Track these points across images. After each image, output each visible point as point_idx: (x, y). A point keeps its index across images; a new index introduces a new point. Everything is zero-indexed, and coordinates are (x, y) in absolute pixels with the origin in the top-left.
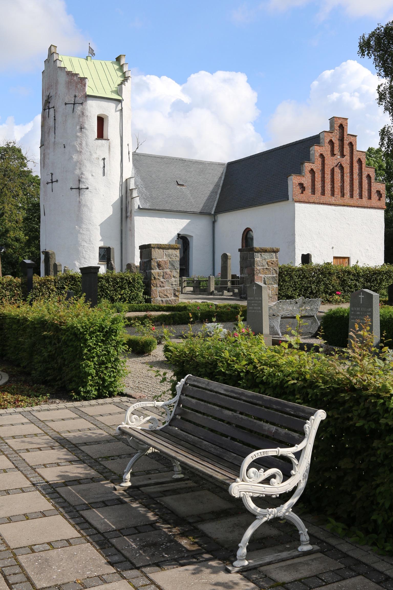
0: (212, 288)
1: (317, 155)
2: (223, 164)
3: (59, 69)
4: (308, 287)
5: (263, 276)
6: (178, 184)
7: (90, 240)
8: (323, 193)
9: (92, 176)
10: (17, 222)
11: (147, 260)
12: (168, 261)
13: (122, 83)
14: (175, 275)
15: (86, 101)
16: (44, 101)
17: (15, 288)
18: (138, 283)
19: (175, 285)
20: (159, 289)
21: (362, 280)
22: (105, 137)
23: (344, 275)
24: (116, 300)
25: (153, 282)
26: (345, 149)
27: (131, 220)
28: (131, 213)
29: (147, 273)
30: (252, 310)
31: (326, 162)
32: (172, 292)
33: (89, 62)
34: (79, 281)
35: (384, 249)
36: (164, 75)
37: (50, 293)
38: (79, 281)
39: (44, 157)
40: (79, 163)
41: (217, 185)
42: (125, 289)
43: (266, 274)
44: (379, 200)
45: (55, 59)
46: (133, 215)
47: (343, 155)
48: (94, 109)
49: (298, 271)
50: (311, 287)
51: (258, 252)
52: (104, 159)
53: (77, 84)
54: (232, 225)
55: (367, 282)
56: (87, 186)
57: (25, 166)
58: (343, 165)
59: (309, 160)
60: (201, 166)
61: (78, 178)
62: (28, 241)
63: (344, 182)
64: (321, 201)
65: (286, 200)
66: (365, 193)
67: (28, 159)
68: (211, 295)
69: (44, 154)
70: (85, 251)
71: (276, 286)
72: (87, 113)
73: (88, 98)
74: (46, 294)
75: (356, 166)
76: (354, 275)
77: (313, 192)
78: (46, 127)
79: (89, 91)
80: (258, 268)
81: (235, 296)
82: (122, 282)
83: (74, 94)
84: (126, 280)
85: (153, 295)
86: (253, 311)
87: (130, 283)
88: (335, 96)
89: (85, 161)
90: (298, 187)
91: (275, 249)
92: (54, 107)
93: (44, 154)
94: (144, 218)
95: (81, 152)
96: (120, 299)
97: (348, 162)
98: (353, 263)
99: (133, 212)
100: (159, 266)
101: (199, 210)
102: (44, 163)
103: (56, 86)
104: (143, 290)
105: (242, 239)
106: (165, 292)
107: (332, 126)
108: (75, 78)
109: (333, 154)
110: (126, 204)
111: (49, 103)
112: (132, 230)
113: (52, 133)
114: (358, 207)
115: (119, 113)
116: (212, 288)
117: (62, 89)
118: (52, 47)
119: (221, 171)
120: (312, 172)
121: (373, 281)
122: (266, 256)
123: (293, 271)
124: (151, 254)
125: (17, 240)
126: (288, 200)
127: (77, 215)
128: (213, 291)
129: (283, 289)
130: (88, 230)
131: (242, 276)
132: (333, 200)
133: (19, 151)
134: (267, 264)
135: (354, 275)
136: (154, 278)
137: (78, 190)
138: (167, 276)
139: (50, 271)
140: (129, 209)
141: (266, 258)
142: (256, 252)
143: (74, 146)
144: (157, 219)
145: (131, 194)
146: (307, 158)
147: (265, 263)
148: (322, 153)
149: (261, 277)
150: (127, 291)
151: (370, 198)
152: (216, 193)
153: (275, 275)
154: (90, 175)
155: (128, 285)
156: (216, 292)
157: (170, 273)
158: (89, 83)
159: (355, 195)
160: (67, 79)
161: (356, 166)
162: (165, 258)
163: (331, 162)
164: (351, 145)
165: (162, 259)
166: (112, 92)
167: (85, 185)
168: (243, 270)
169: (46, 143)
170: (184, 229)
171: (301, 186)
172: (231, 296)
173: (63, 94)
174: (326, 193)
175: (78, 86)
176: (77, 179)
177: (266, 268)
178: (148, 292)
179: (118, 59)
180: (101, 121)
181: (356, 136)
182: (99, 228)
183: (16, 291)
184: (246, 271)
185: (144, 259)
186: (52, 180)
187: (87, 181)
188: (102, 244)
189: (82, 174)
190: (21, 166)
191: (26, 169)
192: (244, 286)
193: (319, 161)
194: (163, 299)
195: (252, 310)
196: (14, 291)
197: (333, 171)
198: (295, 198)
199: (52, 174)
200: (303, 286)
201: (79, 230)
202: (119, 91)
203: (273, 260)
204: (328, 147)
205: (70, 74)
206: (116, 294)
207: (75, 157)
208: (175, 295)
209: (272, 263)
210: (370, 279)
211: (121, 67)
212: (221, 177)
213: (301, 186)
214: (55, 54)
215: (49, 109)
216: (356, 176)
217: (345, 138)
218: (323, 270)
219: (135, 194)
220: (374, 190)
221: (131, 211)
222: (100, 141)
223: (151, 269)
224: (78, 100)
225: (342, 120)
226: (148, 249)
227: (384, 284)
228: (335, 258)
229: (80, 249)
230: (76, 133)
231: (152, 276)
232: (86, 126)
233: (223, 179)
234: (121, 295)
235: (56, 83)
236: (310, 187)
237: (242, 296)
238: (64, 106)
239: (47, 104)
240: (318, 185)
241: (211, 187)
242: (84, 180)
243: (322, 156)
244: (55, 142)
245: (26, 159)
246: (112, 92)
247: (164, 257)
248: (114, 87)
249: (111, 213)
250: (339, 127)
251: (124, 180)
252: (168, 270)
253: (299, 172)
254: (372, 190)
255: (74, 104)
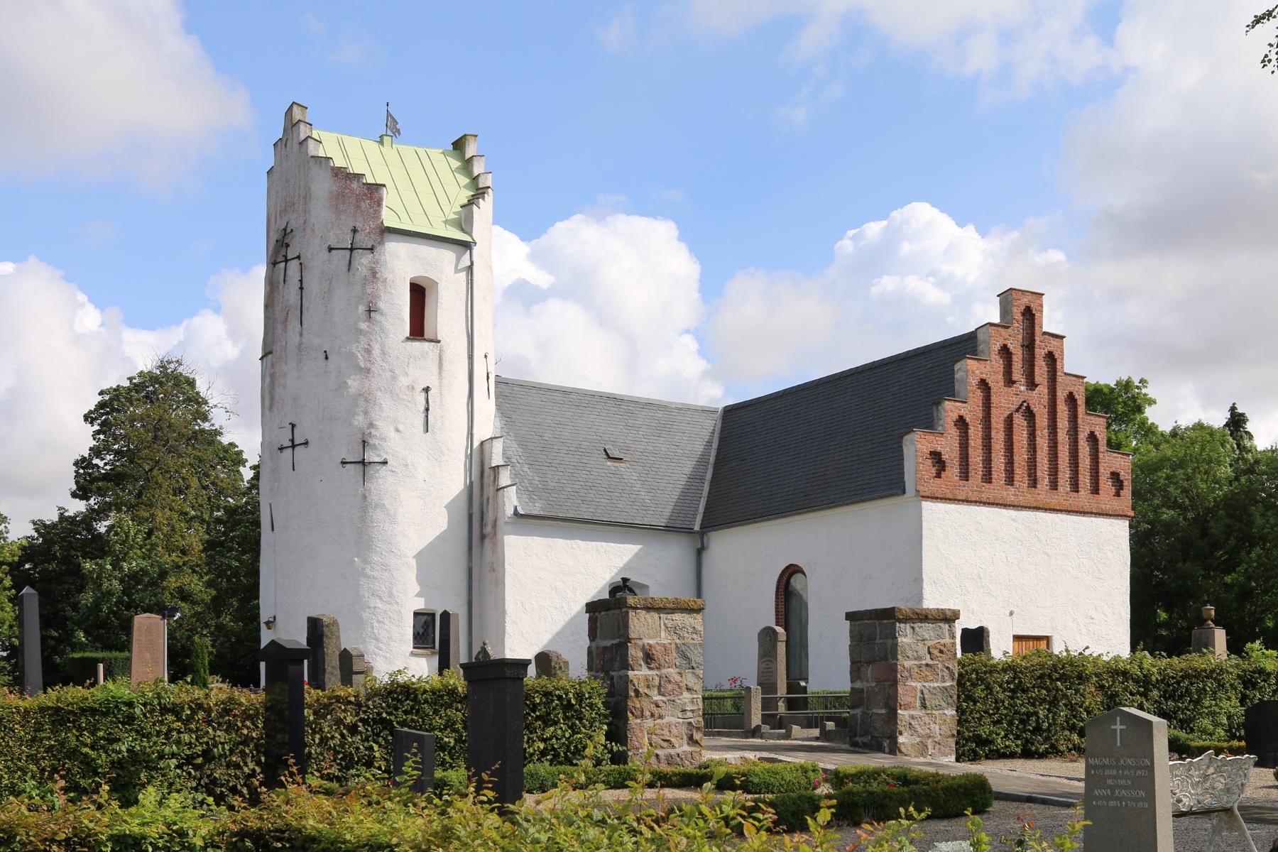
0: (756, 719)
1: (974, 381)
2: (714, 411)
3: (313, 161)
4: (1029, 715)
5: (919, 685)
6: (609, 457)
7: (391, 594)
8: (988, 477)
9: (397, 434)
10: (184, 552)
11: (615, 642)
12: (673, 646)
13: (471, 202)
14: (690, 685)
15: (381, 243)
16: (273, 242)
17: (243, 722)
18: (591, 706)
19: (693, 711)
20: (649, 723)
21: (1155, 693)
22: (428, 333)
23: (1114, 682)
24: (532, 755)
25: (633, 703)
26: (1037, 369)
27: (495, 544)
28: (494, 526)
29: (612, 678)
30: (1108, 798)
31: (994, 399)
32: (684, 730)
33: (386, 149)
34: (426, 701)
35: (1129, 616)
36: (920, 199)
37: (342, 735)
38: (426, 701)
39: (273, 382)
40: (366, 398)
41: (702, 461)
42: (556, 723)
43: (925, 679)
44: (1118, 494)
45: (302, 137)
46: (499, 532)
47: (1032, 385)
48: (402, 263)
49: (1004, 670)
50: (1036, 713)
51: (906, 620)
52: (427, 390)
53: (359, 198)
54: (749, 558)
55: (1166, 699)
56: (385, 456)
57: (205, 419)
58: (1032, 407)
59: (954, 396)
60: (660, 414)
61: (360, 436)
62: (214, 599)
63: (1035, 451)
64: (984, 497)
65: (898, 495)
66: (1085, 479)
67: (211, 403)
68: (753, 737)
69: (272, 375)
70: (379, 622)
71: (951, 712)
72: (384, 273)
73: (387, 236)
74: (333, 738)
75: (1062, 409)
76: (1136, 681)
77: (965, 475)
78: (278, 308)
79: (389, 220)
80: (907, 664)
81: (827, 741)
82: (547, 704)
83: (351, 225)
84: (560, 698)
85: (633, 741)
86: (1112, 803)
87: (569, 706)
88: (888, 283)
89: (379, 393)
90: (929, 462)
91: (949, 614)
92: (299, 257)
93: (272, 375)
94: (529, 539)
95: (368, 371)
96: (543, 753)
97: (1045, 400)
98: (1057, 649)
99: (500, 523)
100: (649, 658)
101: (662, 522)
102: (272, 398)
103: (305, 203)
104: (605, 727)
105: (777, 591)
106: (666, 732)
107: (1005, 311)
108: (355, 185)
109: (1010, 382)
110: (482, 504)
111: (287, 245)
112: (497, 569)
113: (294, 323)
114: (1069, 512)
115: (463, 275)
116: (756, 719)
117: (320, 211)
118: (295, 107)
119: (707, 429)
120: (961, 423)
121: (1181, 697)
122: (926, 630)
123: (991, 672)
124: (626, 626)
125: (184, 595)
126: (904, 492)
127: (359, 529)
128: (758, 727)
129: (966, 721)
130: (386, 567)
131: (858, 685)
132: (1009, 494)
133: (192, 383)
134: (929, 653)
135: (1136, 681)
136: (637, 691)
137: (360, 467)
138: (670, 687)
139: (324, 670)
140: (489, 517)
141: (927, 636)
142: (900, 621)
143: (351, 355)
144: (560, 543)
145: (496, 478)
146: (948, 389)
147: (923, 651)
148: (984, 376)
149: (914, 689)
150: (562, 730)
151: (1095, 490)
152: (702, 479)
153: (948, 684)
154: (392, 429)
155: (564, 713)
156: (766, 729)
157: (678, 678)
158: (389, 198)
159: (1061, 482)
160: (335, 188)
161: (1062, 409)
162: (665, 638)
163: (1005, 401)
164: (1051, 359)
165: (658, 640)
166: (446, 222)
167: (379, 456)
168: (859, 669)
169: (277, 348)
170: (627, 567)
171: (936, 457)
172: (817, 739)
173: (323, 224)
174: (995, 475)
175: (363, 205)
176: (359, 438)
177: (927, 665)
178: (618, 733)
179: (459, 145)
180: (419, 293)
181: (1062, 337)
182: (413, 562)
183: (245, 732)
184: (869, 672)
185: (604, 638)
186: (292, 440)
187: (384, 444)
188: (420, 605)
189: (371, 425)
190: (195, 419)
191: (206, 426)
192: (863, 713)
193: (976, 397)
194: (659, 752)
195: (1108, 798)
196: (239, 729)
197: (1009, 421)
198: (921, 488)
199: (293, 426)
200: (1016, 712)
201: (363, 569)
202: (464, 222)
203: (942, 641)
204: (997, 363)
205: (342, 175)
206: (529, 738)
207: (353, 383)
208: (692, 741)
209: (941, 652)
210: (1175, 690)
211: (467, 164)
212: (710, 443)
213: (936, 457)
214: (302, 126)
215: (286, 261)
216: (1063, 437)
217: (1037, 342)
218: (1063, 667)
219: (505, 478)
220: (1104, 473)
221: (495, 521)
222: (417, 345)
223: (627, 666)
224: (363, 240)
225: (1030, 297)
226: (617, 612)
227: (1207, 704)
228: (1017, 638)
229: (365, 615)
230: (356, 323)
231: (630, 686)
232: (381, 305)
233: (715, 445)
234: (544, 740)
235: (305, 198)
236: (956, 462)
237: (859, 739)
238: (325, 254)
239: (281, 251)
240: (976, 457)
241: (688, 466)
242: (377, 442)
243: (984, 384)
244: (301, 344)
245: (206, 403)
246: (446, 222)
247: (663, 634)
248: (453, 210)
249: (445, 527)
250: (1023, 314)
251: (476, 444)
252: (672, 672)
253: (929, 423)
254: (1101, 470)
255: (352, 250)
